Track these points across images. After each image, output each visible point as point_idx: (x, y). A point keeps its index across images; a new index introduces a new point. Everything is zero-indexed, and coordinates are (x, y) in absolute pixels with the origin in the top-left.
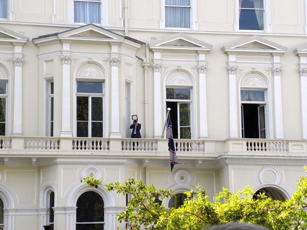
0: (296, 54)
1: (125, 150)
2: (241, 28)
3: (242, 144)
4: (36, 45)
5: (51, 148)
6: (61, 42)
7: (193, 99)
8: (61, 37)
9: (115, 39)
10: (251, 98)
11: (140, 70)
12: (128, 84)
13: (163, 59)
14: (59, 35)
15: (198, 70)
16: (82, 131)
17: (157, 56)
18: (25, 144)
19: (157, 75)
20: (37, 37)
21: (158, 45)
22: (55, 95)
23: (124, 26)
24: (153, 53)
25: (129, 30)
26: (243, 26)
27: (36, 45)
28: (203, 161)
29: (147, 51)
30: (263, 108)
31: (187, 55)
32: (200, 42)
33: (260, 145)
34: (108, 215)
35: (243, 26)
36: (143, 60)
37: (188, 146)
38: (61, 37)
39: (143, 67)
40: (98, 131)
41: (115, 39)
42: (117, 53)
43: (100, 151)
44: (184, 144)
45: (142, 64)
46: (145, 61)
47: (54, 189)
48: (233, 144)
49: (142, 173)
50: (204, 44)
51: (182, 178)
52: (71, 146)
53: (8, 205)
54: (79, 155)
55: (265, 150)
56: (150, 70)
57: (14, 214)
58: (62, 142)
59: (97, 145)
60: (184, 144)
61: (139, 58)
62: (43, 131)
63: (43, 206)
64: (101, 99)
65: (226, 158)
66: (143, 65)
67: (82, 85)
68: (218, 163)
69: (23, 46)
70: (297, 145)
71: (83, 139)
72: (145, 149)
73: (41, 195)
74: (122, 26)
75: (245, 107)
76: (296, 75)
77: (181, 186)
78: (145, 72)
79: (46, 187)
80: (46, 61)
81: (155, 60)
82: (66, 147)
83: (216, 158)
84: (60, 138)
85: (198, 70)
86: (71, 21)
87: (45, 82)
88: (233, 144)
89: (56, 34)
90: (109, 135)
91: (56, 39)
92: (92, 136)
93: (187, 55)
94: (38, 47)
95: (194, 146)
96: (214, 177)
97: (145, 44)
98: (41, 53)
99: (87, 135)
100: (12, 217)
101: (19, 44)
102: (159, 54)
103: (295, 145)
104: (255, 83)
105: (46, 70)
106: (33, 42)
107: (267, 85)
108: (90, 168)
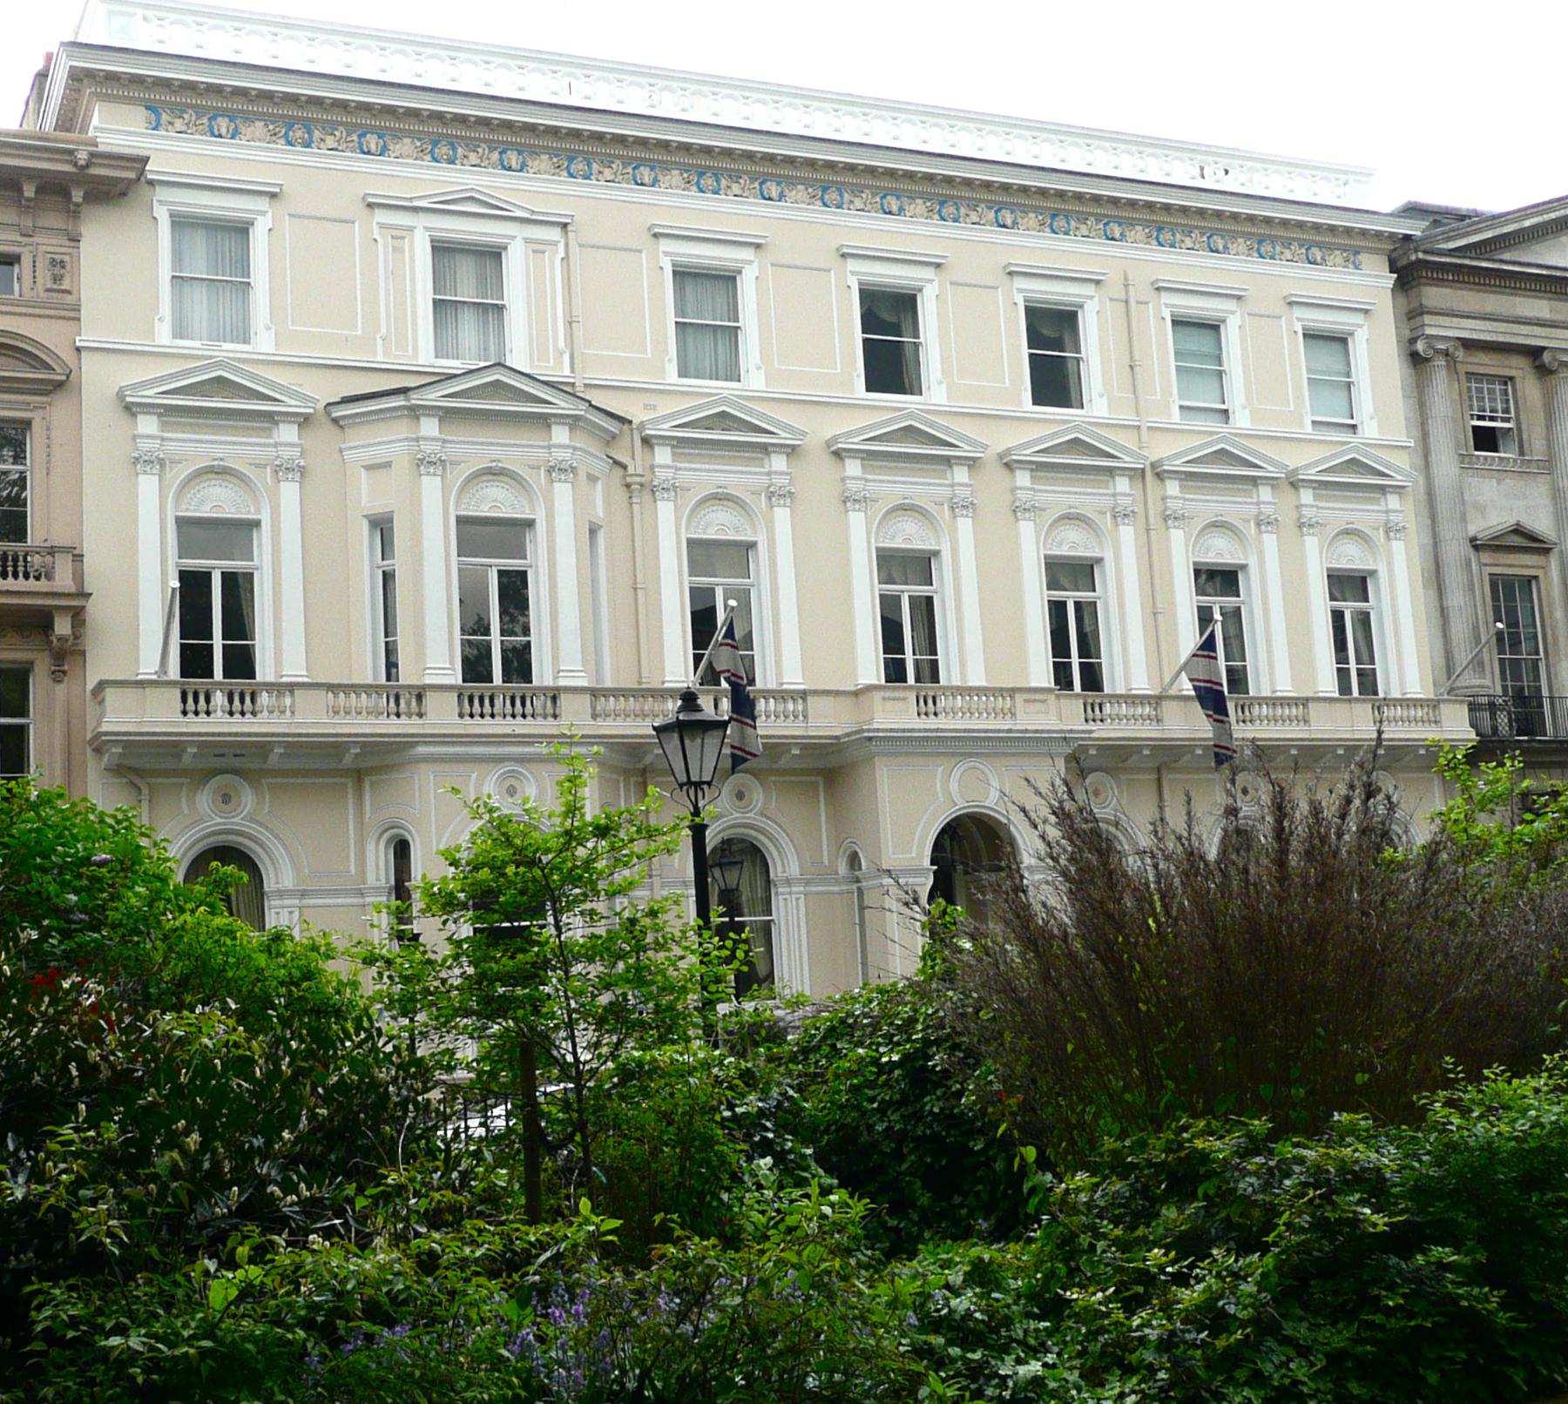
0: (833, 449)
1: (191, 715)
2: (869, 389)
3: (904, 699)
4: (335, 421)
5: (505, 716)
6: (415, 412)
7: (1249, 595)
8: (416, 399)
9: (563, 405)
10: (896, 577)
11: (622, 494)
12: (593, 532)
13: (679, 465)
14: (413, 395)
15: (770, 498)
16: (195, 662)
17: (663, 455)
18: (594, 708)
19: (665, 510)
20: (338, 400)
21: (1313, 471)
22: (399, 563)
23: (573, 370)
24: (651, 447)
25: (587, 382)
26: (876, 382)
27: (335, 421)
28: (804, 747)
29: (638, 442)
30: (249, 577)
31: (886, 467)
32: (773, 421)
33: (518, 702)
34: (278, 913)
35: (876, 382)
36: (625, 467)
37: (523, 704)
38: (416, 399)
39: (628, 486)
40: (241, 663)
41: (563, 405)
42: (568, 447)
43: (491, 721)
44: (1092, 705)
45: (624, 477)
46: (631, 470)
47: (410, 833)
48: (1026, 701)
49: (635, 783)
50: (969, 441)
51: (740, 796)
52: (180, 706)
53: (277, 875)
54: (444, 735)
55: (936, 714)
56: (647, 495)
57: (297, 902)
58: (564, 699)
59: (520, 704)
60: (1092, 705)
61: (616, 462)
62: (369, 670)
63: (378, 880)
64: (523, 575)
65: (870, 739)
66: (629, 480)
67: (193, 532)
68: (840, 751)
69: (788, 455)
70: (1035, 701)
71: (477, 687)
72: (243, 714)
73: (370, 847)
74: (567, 372)
75: (184, 576)
76: (1296, 530)
77: (220, 824)
78: (634, 500)
79: (383, 828)
80: (368, 468)
81: (658, 466)
82: (443, 715)
83: (836, 737)
84: (558, 689)
85: (770, 498)
86: (424, 355)
87: (365, 525)
88: (1026, 701)
89: (404, 391)
90: (556, 678)
91: (403, 403)
92: (1083, 689)
93: (886, 467)
94: (341, 427)
95: (264, 699)
96: (822, 794)
97: (630, 422)
98: (352, 444)
99: (209, 673)
100: (291, 913)
101: (289, 417)
102: (1176, 483)
103: (889, 699)
104: (218, 501)
105: (368, 496)
106: (328, 414)
107: (1375, 561)
108: (505, 773)
